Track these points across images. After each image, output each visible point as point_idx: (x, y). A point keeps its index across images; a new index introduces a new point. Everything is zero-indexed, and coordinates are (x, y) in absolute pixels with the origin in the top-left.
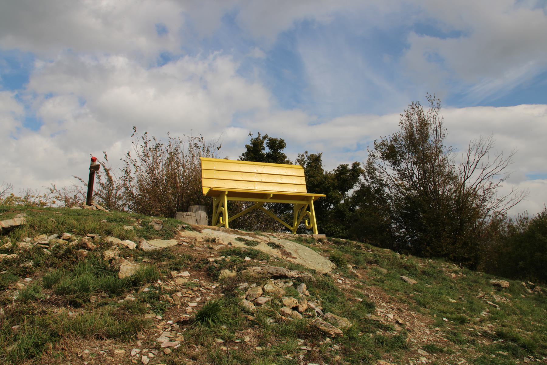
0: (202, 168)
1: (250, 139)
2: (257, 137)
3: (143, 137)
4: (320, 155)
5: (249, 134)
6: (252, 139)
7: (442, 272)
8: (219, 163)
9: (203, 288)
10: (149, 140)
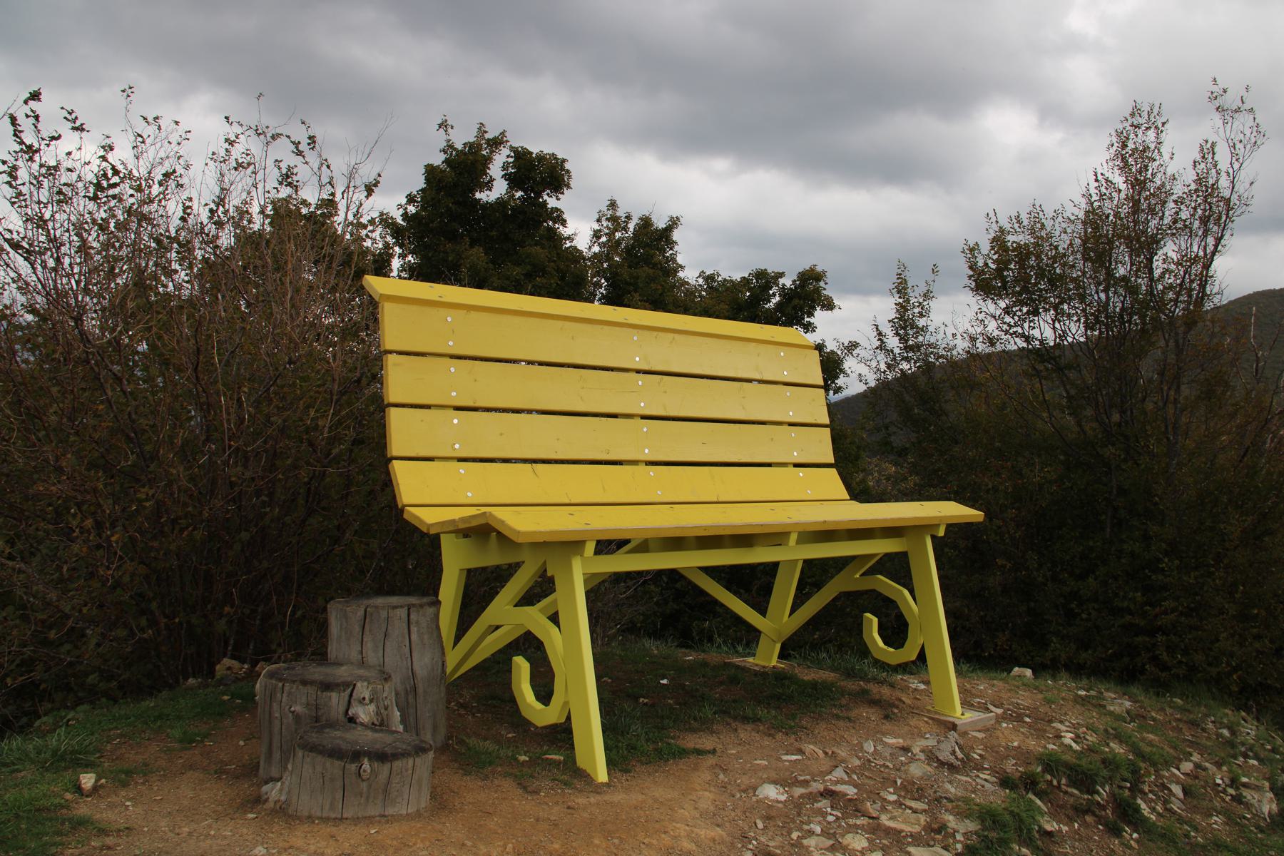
0: (388, 346)
1: (443, 144)
2: (472, 140)
3: (13, 120)
4: (674, 223)
5: (440, 126)
6: (451, 146)
7: (1097, 235)
8: (473, 314)
9: (1262, 305)
10: (53, 138)
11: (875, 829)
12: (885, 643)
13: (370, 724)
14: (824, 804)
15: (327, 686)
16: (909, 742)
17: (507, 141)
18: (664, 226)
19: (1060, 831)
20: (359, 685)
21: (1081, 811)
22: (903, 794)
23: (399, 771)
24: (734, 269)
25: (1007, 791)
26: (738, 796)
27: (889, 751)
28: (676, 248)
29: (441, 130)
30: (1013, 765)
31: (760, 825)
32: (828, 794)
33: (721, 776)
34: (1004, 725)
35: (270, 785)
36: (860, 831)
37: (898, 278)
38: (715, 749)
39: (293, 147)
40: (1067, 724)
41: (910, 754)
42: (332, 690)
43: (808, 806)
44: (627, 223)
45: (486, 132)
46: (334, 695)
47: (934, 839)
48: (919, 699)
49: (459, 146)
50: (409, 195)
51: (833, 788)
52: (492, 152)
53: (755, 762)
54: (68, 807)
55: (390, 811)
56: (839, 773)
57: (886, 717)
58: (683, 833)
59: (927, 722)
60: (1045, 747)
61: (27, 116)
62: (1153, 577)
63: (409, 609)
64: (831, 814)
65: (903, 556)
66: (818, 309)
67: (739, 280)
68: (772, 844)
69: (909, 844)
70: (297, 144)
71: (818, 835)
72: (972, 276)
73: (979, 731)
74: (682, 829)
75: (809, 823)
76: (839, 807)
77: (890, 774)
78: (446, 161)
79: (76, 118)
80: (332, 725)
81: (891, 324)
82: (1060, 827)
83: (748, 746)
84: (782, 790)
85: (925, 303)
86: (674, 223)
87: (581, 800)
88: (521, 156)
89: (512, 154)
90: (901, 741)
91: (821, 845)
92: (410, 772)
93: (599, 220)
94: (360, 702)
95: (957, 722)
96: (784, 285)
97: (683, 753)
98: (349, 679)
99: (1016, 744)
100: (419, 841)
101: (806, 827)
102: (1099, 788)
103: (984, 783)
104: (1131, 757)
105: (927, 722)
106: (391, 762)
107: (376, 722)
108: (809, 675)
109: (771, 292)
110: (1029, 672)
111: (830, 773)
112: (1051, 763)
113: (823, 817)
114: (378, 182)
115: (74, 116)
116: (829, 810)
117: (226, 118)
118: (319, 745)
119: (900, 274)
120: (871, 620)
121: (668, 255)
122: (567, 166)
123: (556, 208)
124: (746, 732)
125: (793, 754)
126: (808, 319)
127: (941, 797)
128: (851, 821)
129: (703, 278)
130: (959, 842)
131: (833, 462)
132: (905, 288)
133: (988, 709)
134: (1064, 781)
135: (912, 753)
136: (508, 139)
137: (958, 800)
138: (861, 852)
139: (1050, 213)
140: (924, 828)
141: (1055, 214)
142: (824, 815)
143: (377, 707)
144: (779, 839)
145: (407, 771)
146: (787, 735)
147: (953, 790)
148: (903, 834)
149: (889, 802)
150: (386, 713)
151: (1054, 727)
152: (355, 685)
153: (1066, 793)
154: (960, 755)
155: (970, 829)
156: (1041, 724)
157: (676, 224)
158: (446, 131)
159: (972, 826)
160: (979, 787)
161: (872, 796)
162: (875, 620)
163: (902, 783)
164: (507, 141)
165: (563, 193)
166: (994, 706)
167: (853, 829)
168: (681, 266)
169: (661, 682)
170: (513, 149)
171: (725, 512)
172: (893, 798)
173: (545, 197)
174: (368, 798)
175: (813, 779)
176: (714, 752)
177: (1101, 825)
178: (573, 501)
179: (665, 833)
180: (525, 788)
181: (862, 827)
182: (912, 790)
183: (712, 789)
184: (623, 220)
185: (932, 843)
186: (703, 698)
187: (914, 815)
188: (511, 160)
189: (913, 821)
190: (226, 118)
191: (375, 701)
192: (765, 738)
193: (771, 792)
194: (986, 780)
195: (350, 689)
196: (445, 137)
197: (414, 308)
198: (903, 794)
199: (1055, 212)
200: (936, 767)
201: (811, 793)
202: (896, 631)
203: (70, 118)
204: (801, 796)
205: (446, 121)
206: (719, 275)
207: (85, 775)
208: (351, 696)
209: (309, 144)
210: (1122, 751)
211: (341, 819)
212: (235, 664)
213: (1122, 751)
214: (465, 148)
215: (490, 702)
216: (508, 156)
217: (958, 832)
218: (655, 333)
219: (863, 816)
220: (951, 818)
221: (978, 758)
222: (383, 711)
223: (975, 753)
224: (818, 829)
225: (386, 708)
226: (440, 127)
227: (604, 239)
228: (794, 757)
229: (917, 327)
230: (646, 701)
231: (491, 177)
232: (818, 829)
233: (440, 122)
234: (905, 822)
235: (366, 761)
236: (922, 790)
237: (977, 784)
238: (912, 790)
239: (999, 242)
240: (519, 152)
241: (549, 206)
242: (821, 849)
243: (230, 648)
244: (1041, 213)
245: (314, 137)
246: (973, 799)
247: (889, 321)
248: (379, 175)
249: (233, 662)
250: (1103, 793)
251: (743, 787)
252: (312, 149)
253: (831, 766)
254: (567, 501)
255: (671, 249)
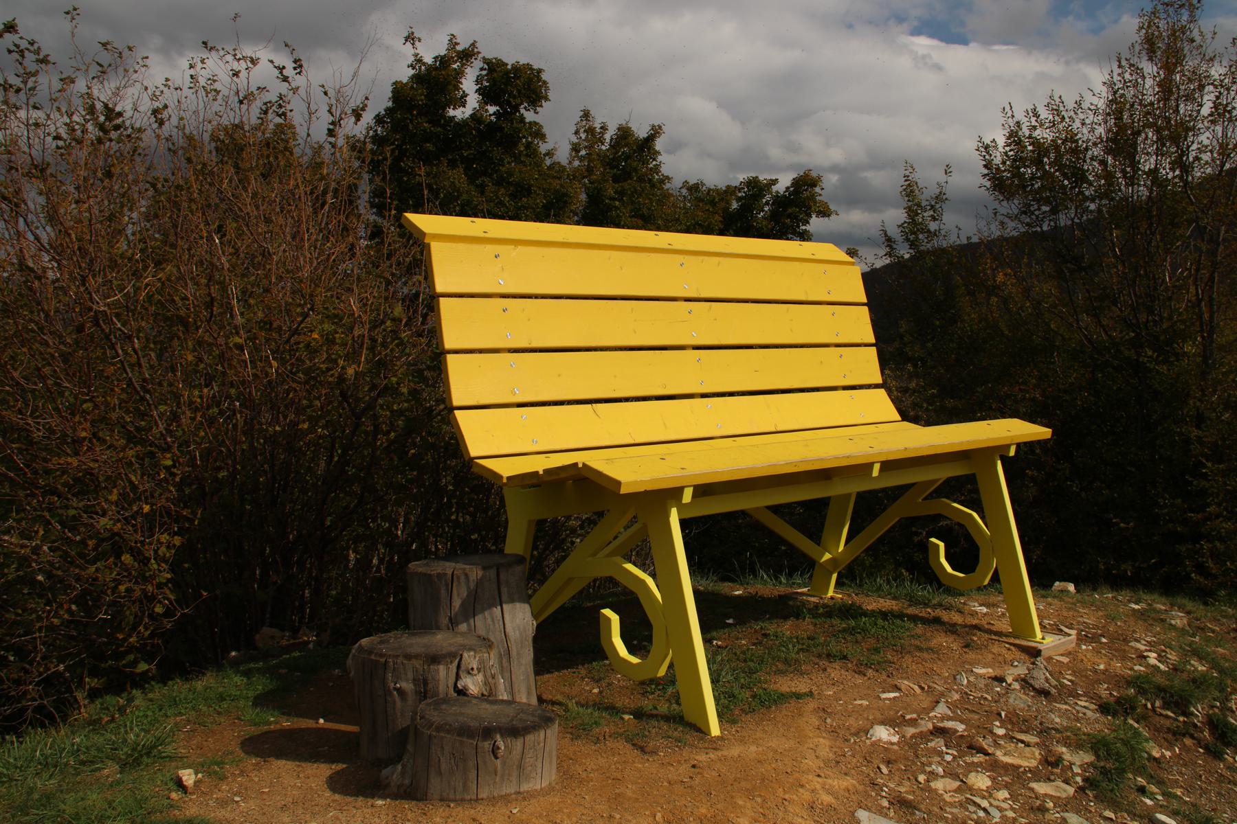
1: (411, 59)
2: (443, 52)
4: (656, 132)
6: (419, 61)
11: (994, 767)
12: (954, 569)
13: (480, 696)
14: (938, 743)
15: (434, 659)
16: (998, 673)
17: (479, 53)
18: (646, 135)
19: (1163, 756)
20: (465, 655)
21: (1177, 734)
22: (1009, 727)
23: (532, 745)
24: (715, 176)
25: (1109, 718)
26: (852, 741)
27: (983, 682)
28: (660, 158)
29: (408, 43)
30: (1105, 690)
31: (885, 770)
32: (939, 732)
33: (829, 721)
34: (1084, 647)
35: (389, 769)
36: (980, 770)
37: (906, 181)
38: (811, 692)
39: (277, 72)
40: (1144, 642)
41: (1004, 684)
42: (439, 663)
43: (922, 746)
44: (602, 134)
45: (457, 44)
46: (442, 668)
47: (1052, 773)
48: (993, 624)
49: (429, 59)
50: (378, 115)
51: (941, 725)
52: (463, 65)
53: (856, 702)
54: (179, 808)
55: (525, 787)
56: (942, 709)
57: (967, 646)
58: (818, 786)
59: (1009, 649)
60: (1131, 669)
61: (10, 52)
62: (1195, 483)
63: (498, 569)
64: (947, 753)
65: (971, 479)
66: (814, 216)
67: (724, 189)
68: (902, 789)
69: (1030, 780)
70: (281, 69)
71: (942, 777)
72: (988, 175)
73: (1062, 655)
74: (817, 783)
75: (930, 764)
76: (952, 745)
77: (991, 707)
78: (413, 77)
79: (39, 48)
80: (446, 700)
81: (901, 229)
82: (1162, 753)
83: (842, 686)
84: (892, 730)
85: (938, 206)
86: (656, 132)
87: (702, 758)
88: (494, 67)
89: (486, 66)
90: (990, 670)
91: (948, 788)
92: (542, 744)
93: (577, 133)
94: (469, 673)
95: (1040, 647)
96: (777, 192)
97: (783, 698)
98: (453, 649)
99: (1102, 667)
100: (565, 817)
101: (928, 769)
102: (1192, 709)
103: (1085, 710)
104: (1215, 675)
105: (1009, 649)
106: (524, 735)
107: (485, 693)
108: (873, 604)
109: (764, 201)
110: (1071, 587)
111: (933, 709)
112: (1136, 682)
113: (940, 756)
114: (366, 106)
115: (36, 46)
116: (944, 748)
117: (204, 43)
118: (446, 724)
119: (908, 176)
120: (938, 546)
121: (651, 166)
122: (544, 77)
123: (535, 122)
124: (836, 671)
125: (889, 692)
126: (804, 228)
127: (1048, 728)
128: (968, 759)
129: (688, 189)
130: (1078, 774)
131: (881, 382)
132: (912, 191)
133: (1062, 631)
134: (1158, 704)
135: (1006, 683)
136: (479, 50)
137: (1067, 731)
138: (986, 791)
139: (1070, 104)
140: (1040, 763)
141: (1076, 106)
142: (941, 754)
143: (485, 676)
144: (907, 783)
145: (539, 744)
146: (877, 671)
147: (1057, 720)
148: (1022, 769)
149: (999, 736)
150: (493, 682)
151: (1132, 647)
152: (461, 655)
153: (1161, 715)
154: (1054, 682)
155: (1086, 761)
156: (1119, 644)
157: (658, 133)
158: (413, 44)
159: (1088, 758)
160: (1081, 715)
161: (981, 730)
162: (942, 545)
163: (1006, 715)
164: (479, 53)
165: (541, 106)
166: (1066, 627)
167: (972, 767)
168: (668, 178)
169: (727, 621)
170: (485, 60)
171: (807, 445)
172: (1001, 732)
173: (522, 111)
174: (502, 776)
175: (919, 716)
176: (810, 694)
177: (1201, 747)
178: (638, 441)
179: (802, 786)
180: (642, 749)
181: (980, 764)
182: (1016, 722)
183: (824, 735)
184: (599, 131)
185: (1052, 777)
186: (777, 637)
187: (1027, 749)
188: (484, 73)
189: (1027, 755)
190: (204, 43)
191: (482, 670)
192: (856, 676)
193: (883, 734)
194: (1085, 707)
195: (457, 660)
196: (412, 51)
197: (461, 246)
198: (1009, 727)
199: (1076, 103)
200: (1033, 696)
201: (921, 732)
202: (965, 556)
203: (32, 48)
204: (913, 736)
205: (413, 33)
206: (703, 184)
207: (183, 771)
208: (459, 667)
209: (295, 69)
210: (1204, 668)
211: (477, 800)
212: (275, 632)
213: (1204, 668)
214: (436, 62)
215: (558, 655)
216: (482, 69)
217: (1074, 764)
218: (701, 258)
219: (977, 753)
220: (1064, 749)
221: (1070, 684)
222: (490, 680)
223: (1065, 678)
224: (940, 770)
225: (493, 678)
226: (406, 41)
227: (583, 153)
228: (892, 695)
229: (929, 231)
230: (720, 643)
231: (464, 92)
232: (940, 770)
233: (407, 34)
234: (1021, 756)
235: (498, 737)
236: (1027, 721)
237: (1078, 712)
238: (1016, 722)
239: (1014, 137)
240: (491, 62)
241: (527, 120)
242: (950, 791)
243: (268, 616)
244: (1061, 104)
245: (300, 60)
246: (1079, 729)
247: (899, 226)
248: (367, 98)
249: (273, 630)
250: (1199, 711)
251: (853, 730)
252: (299, 73)
253: (931, 702)
254: (632, 442)
255: (654, 160)
